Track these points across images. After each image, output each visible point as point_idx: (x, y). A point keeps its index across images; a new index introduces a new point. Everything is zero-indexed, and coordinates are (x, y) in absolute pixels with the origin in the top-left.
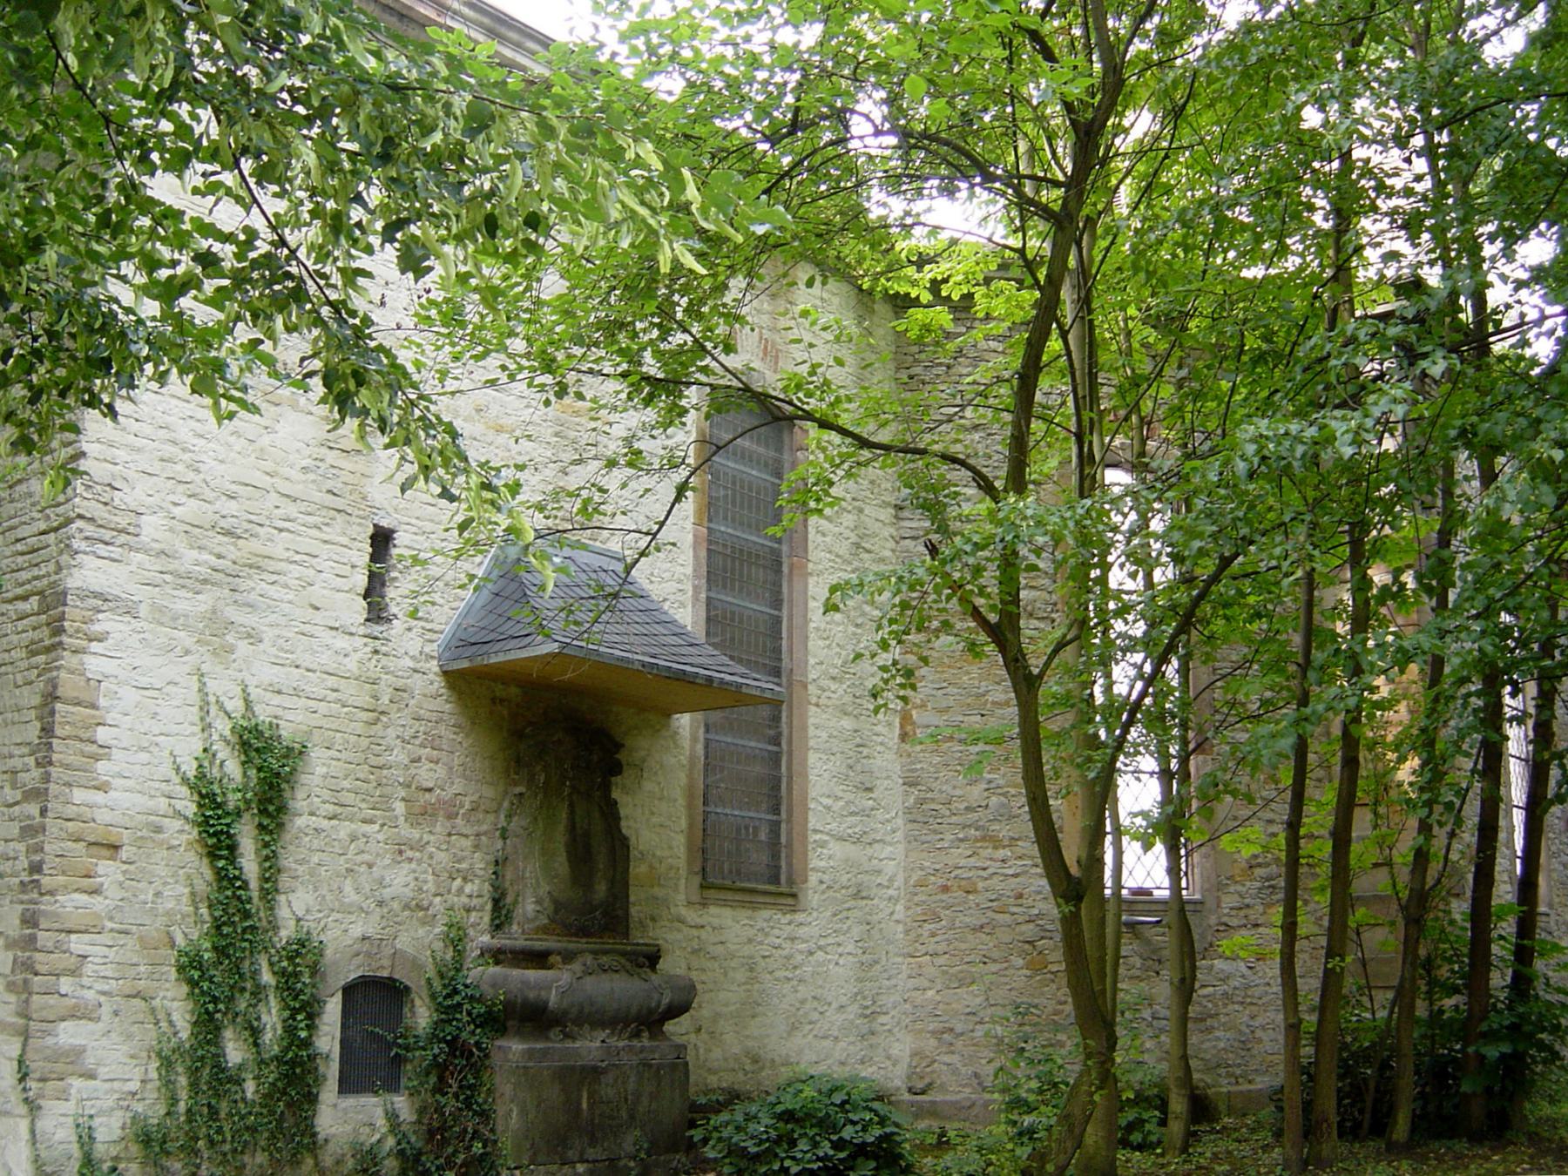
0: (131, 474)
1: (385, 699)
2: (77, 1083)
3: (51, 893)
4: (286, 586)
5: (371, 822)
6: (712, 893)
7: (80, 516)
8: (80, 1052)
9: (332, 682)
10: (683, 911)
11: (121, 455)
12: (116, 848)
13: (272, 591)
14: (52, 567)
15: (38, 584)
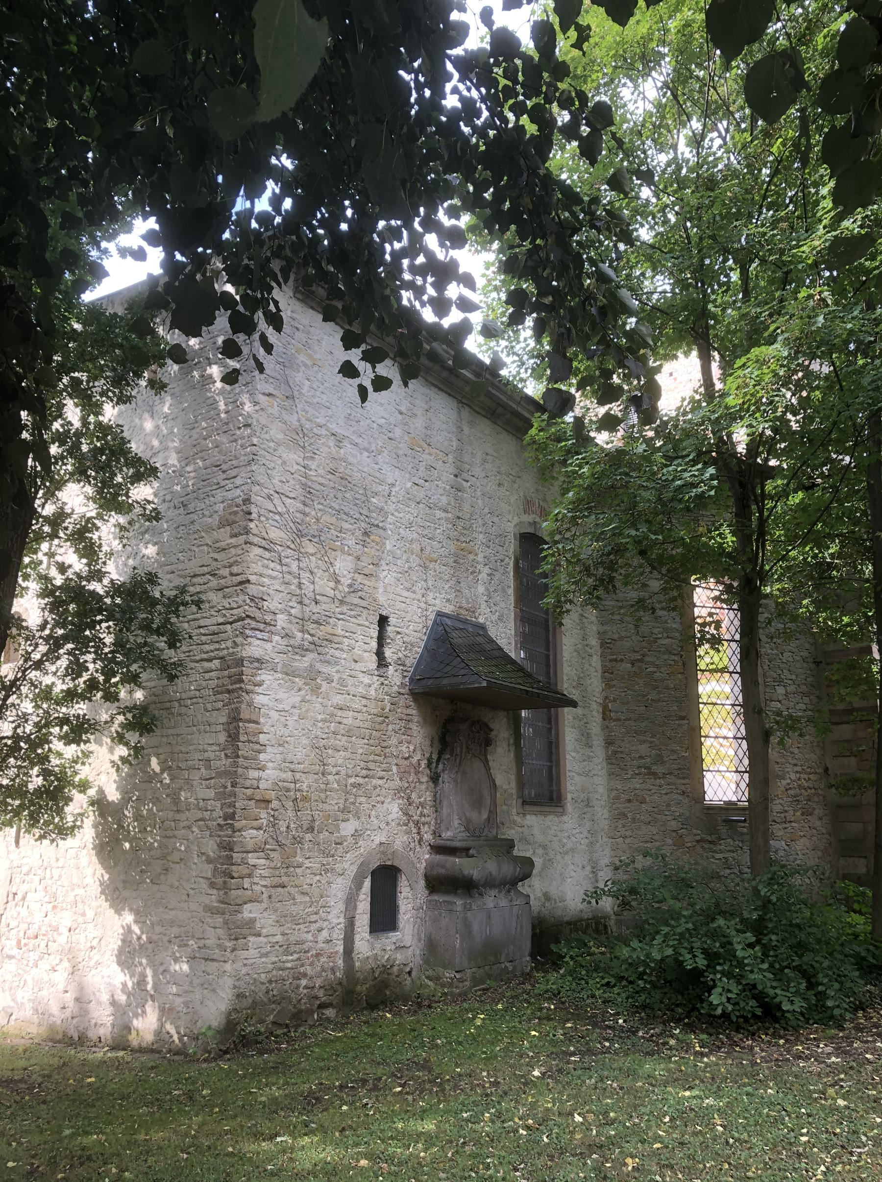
0: (271, 592)
1: (387, 710)
2: (252, 939)
3: (239, 831)
4: (342, 650)
5: (382, 778)
6: (528, 808)
7: (248, 616)
8: (253, 921)
9: (364, 701)
10: (516, 818)
11: (266, 580)
12: (269, 802)
13: (337, 653)
14: (229, 644)
15: (221, 654)
